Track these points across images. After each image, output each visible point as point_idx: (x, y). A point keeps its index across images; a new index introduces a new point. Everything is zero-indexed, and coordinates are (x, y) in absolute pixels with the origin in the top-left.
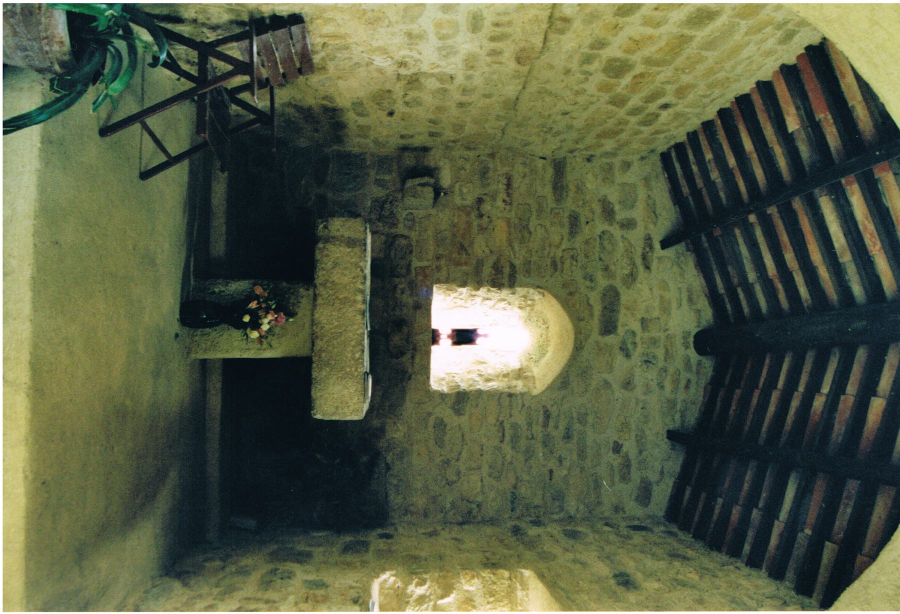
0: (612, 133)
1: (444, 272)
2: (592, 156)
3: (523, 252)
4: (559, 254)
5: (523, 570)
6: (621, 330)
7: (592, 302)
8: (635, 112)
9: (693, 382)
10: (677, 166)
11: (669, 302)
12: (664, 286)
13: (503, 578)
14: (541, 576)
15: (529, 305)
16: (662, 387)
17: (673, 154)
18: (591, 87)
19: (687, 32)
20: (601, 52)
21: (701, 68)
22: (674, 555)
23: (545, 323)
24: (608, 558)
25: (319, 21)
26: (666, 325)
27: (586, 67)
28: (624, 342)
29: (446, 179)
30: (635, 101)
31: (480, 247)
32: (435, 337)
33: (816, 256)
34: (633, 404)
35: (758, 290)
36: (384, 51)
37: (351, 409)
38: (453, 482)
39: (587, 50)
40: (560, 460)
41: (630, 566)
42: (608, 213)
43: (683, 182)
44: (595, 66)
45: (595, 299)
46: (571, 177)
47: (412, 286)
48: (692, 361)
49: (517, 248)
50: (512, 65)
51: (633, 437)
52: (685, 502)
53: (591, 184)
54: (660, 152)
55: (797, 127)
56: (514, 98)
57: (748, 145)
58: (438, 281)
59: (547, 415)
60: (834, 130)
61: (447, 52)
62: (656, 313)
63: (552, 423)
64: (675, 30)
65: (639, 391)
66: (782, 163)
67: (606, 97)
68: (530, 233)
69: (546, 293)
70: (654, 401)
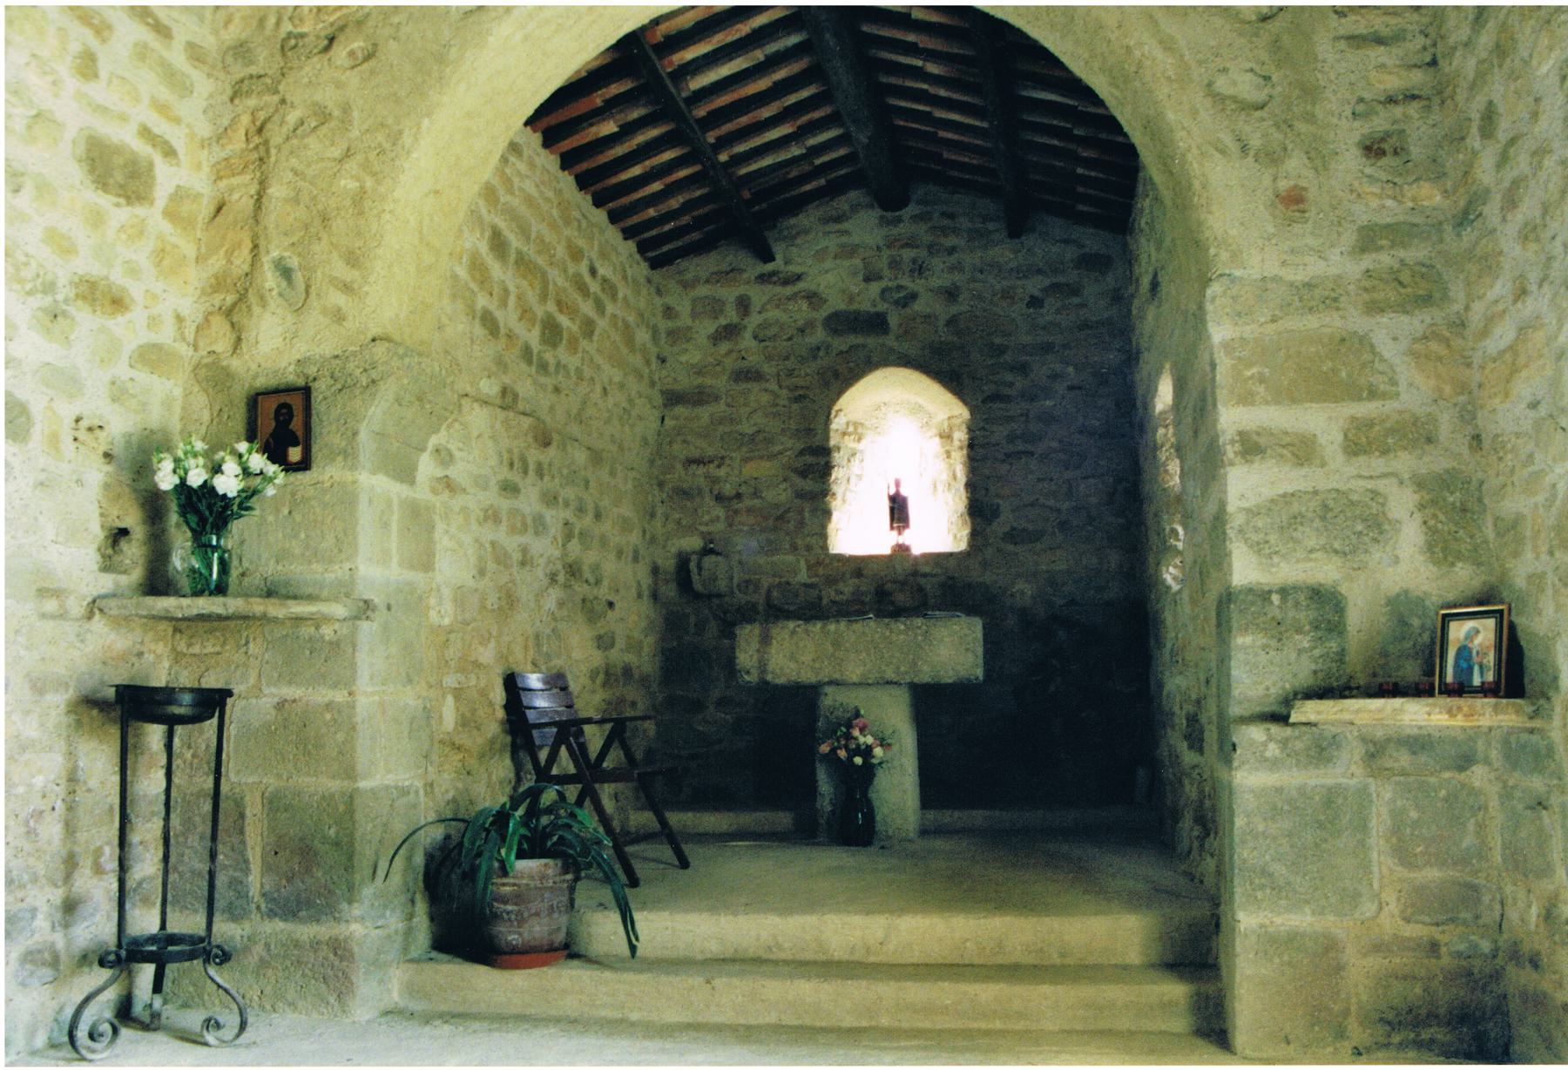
1: (813, 541)
2: (658, 357)
3: (784, 439)
4: (785, 392)
6: (882, 307)
7: (844, 348)
8: (600, 307)
10: (665, 248)
11: (843, 246)
12: (821, 255)
13: (1166, 435)
15: (856, 429)
16: (952, 250)
17: (651, 254)
19: (513, 258)
20: (535, 351)
21: (550, 237)
23: (878, 408)
25: (511, 659)
26: (871, 248)
27: (552, 369)
28: (896, 302)
29: (693, 543)
30: (587, 308)
31: (780, 494)
32: (902, 549)
33: (763, 84)
34: (978, 285)
35: (813, 141)
36: (539, 595)
37: (968, 632)
39: (534, 369)
40: (1054, 377)
42: (729, 332)
43: (687, 239)
44: (549, 357)
45: (841, 343)
46: (685, 382)
47: (831, 581)
48: (917, 212)
49: (779, 448)
50: (552, 451)
51: (1019, 283)
52: (1091, 210)
53: (694, 356)
55: (612, 123)
57: (636, 171)
58: (825, 547)
60: (613, 86)
61: (539, 525)
62: (857, 261)
63: (1007, 391)
64: (510, 273)
66: (653, 133)
67: (584, 343)
69: (836, 408)
70: (971, 259)
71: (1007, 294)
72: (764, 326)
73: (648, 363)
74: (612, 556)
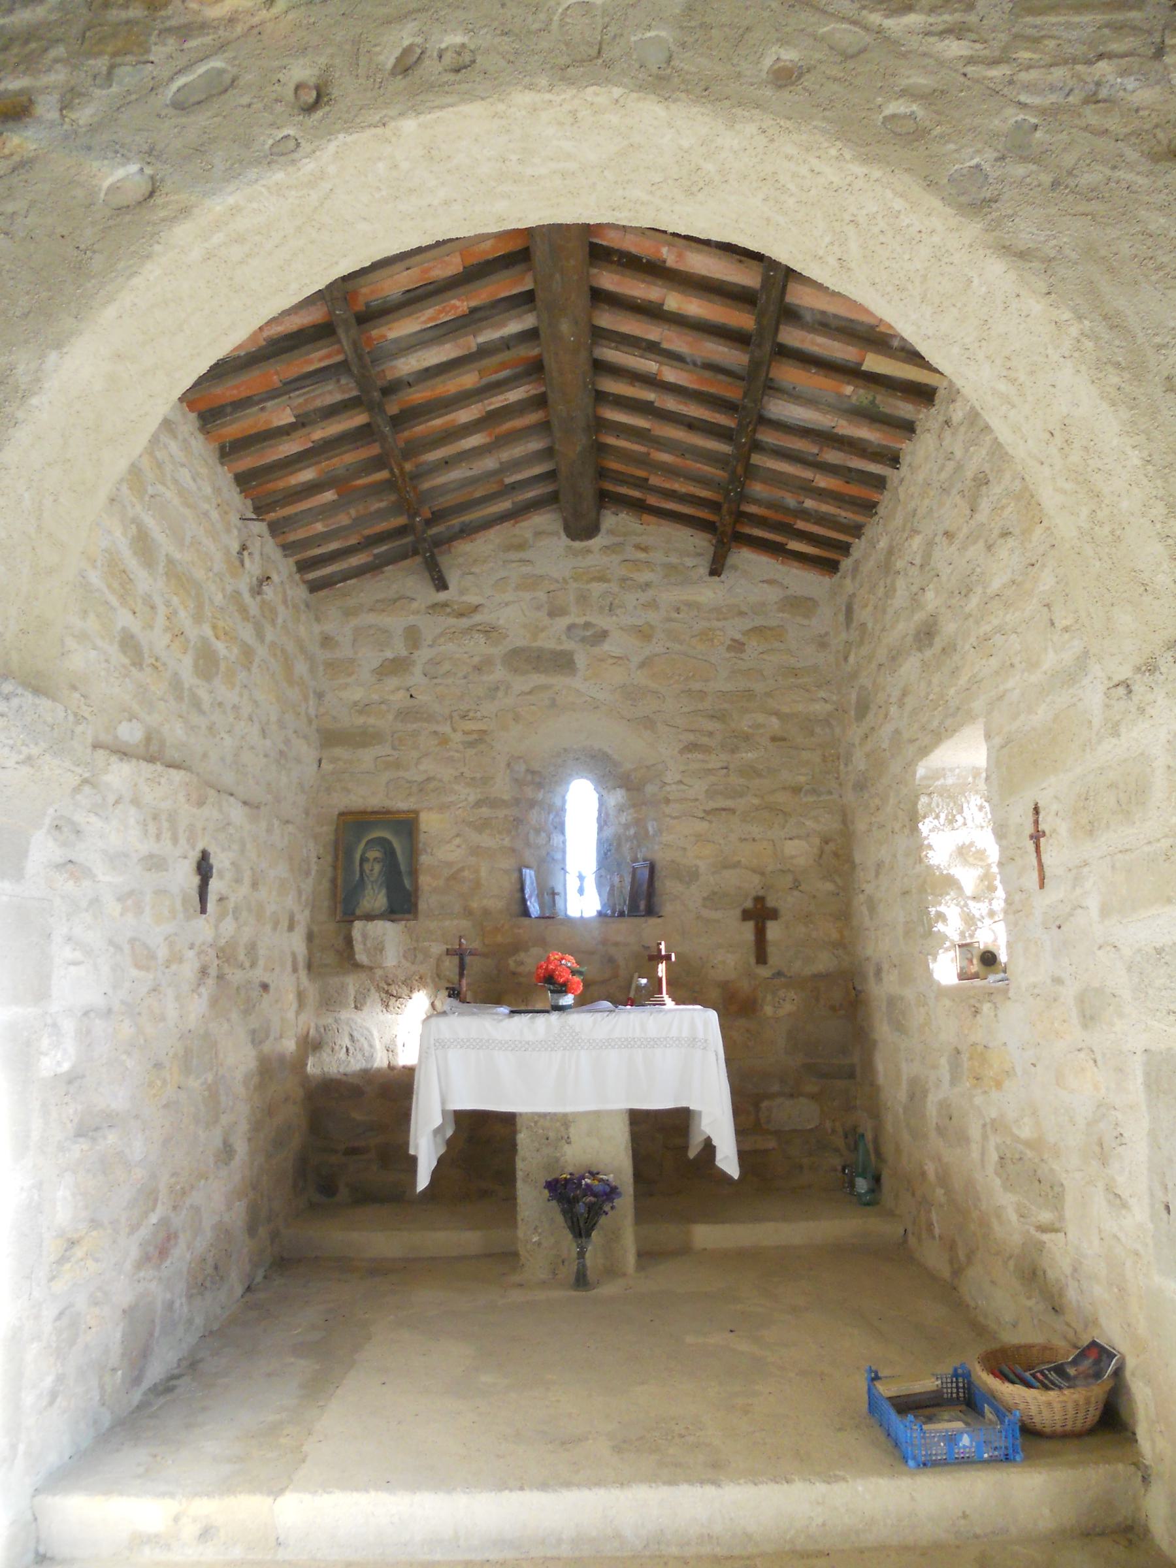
0: (288, 667)
5: (918, 776)
6: (568, 645)
7: (526, 688)
8: (261, 636)
9: (638, 540)
13: (929, 804)
14: (925, 751)
16: (647, 585)
18: (230, 696)
20: (186, 686)
22: (886, 567)
24: (895, 657)
27: (206, 706)
30: (247, 633)
38: (796, 880)
41: (904, 628)
42: (397, 666)
45: (521, 683)
49: (453, 798)
51: (719, 624)
54: (308, 593)
56: (246, 809)
59: (692, 747)
62: (541, 595)
63: (705, 740)
65: (652, 617)
67: (242, 675)
68: (429, 779)
70: (670, 596)
71: (706, 636)
72: (435, 662)
73: (306, 698)
74: (268, 928)
